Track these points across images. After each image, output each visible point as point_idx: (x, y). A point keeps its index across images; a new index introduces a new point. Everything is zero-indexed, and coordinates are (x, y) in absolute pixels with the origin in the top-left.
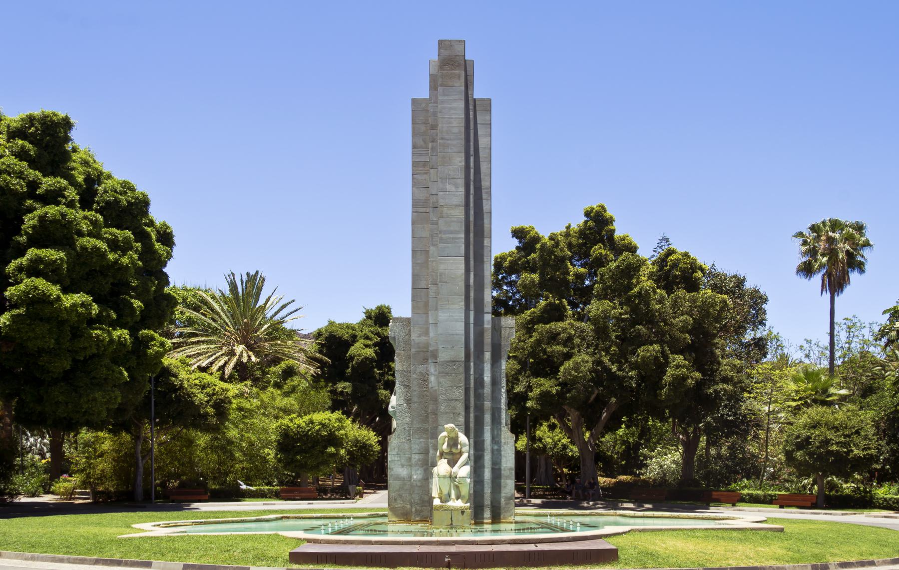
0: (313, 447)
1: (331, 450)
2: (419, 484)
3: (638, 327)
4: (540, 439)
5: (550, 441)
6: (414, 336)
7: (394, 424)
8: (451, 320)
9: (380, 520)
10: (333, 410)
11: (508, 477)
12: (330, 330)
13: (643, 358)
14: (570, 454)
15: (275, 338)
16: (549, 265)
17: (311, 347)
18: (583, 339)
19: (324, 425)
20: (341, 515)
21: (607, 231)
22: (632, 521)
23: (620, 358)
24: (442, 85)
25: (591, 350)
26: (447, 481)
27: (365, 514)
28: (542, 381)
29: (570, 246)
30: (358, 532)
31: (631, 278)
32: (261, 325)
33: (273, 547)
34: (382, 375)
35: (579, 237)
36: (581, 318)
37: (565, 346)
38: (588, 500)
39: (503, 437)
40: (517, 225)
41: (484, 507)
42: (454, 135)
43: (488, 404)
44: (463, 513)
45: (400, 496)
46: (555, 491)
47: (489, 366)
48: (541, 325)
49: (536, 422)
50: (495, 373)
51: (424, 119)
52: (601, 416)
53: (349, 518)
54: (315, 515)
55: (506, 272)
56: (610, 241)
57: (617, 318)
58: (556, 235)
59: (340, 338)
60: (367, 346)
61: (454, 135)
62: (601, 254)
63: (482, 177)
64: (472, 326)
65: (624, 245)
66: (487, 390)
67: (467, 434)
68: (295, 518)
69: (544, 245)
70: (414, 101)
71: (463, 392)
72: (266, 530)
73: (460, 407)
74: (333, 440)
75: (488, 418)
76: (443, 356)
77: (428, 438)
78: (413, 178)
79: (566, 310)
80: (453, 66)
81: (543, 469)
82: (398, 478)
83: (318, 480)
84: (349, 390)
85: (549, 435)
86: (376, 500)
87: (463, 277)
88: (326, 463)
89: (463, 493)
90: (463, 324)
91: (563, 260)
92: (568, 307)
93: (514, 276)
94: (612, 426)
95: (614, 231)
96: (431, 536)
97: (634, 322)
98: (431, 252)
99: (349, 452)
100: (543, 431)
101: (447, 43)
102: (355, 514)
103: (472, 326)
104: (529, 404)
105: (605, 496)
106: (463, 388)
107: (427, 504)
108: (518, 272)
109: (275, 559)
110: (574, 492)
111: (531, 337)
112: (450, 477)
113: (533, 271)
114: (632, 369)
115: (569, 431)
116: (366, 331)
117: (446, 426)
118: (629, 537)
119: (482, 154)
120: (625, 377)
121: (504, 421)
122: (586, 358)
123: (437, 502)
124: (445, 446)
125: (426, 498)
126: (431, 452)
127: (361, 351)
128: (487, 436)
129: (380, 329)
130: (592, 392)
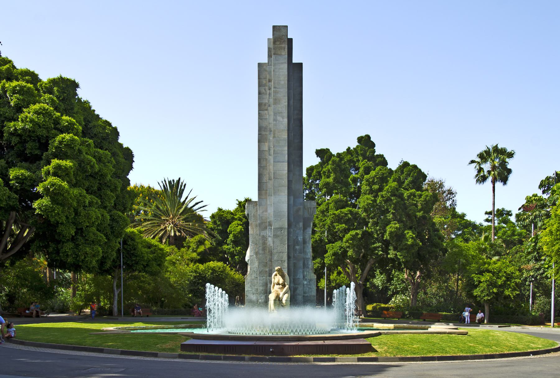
8: (280, 201)
49: (330, 271)
76: (275, 225)
78: (259, 113)
80: (281, 41)
101: (278, 28)
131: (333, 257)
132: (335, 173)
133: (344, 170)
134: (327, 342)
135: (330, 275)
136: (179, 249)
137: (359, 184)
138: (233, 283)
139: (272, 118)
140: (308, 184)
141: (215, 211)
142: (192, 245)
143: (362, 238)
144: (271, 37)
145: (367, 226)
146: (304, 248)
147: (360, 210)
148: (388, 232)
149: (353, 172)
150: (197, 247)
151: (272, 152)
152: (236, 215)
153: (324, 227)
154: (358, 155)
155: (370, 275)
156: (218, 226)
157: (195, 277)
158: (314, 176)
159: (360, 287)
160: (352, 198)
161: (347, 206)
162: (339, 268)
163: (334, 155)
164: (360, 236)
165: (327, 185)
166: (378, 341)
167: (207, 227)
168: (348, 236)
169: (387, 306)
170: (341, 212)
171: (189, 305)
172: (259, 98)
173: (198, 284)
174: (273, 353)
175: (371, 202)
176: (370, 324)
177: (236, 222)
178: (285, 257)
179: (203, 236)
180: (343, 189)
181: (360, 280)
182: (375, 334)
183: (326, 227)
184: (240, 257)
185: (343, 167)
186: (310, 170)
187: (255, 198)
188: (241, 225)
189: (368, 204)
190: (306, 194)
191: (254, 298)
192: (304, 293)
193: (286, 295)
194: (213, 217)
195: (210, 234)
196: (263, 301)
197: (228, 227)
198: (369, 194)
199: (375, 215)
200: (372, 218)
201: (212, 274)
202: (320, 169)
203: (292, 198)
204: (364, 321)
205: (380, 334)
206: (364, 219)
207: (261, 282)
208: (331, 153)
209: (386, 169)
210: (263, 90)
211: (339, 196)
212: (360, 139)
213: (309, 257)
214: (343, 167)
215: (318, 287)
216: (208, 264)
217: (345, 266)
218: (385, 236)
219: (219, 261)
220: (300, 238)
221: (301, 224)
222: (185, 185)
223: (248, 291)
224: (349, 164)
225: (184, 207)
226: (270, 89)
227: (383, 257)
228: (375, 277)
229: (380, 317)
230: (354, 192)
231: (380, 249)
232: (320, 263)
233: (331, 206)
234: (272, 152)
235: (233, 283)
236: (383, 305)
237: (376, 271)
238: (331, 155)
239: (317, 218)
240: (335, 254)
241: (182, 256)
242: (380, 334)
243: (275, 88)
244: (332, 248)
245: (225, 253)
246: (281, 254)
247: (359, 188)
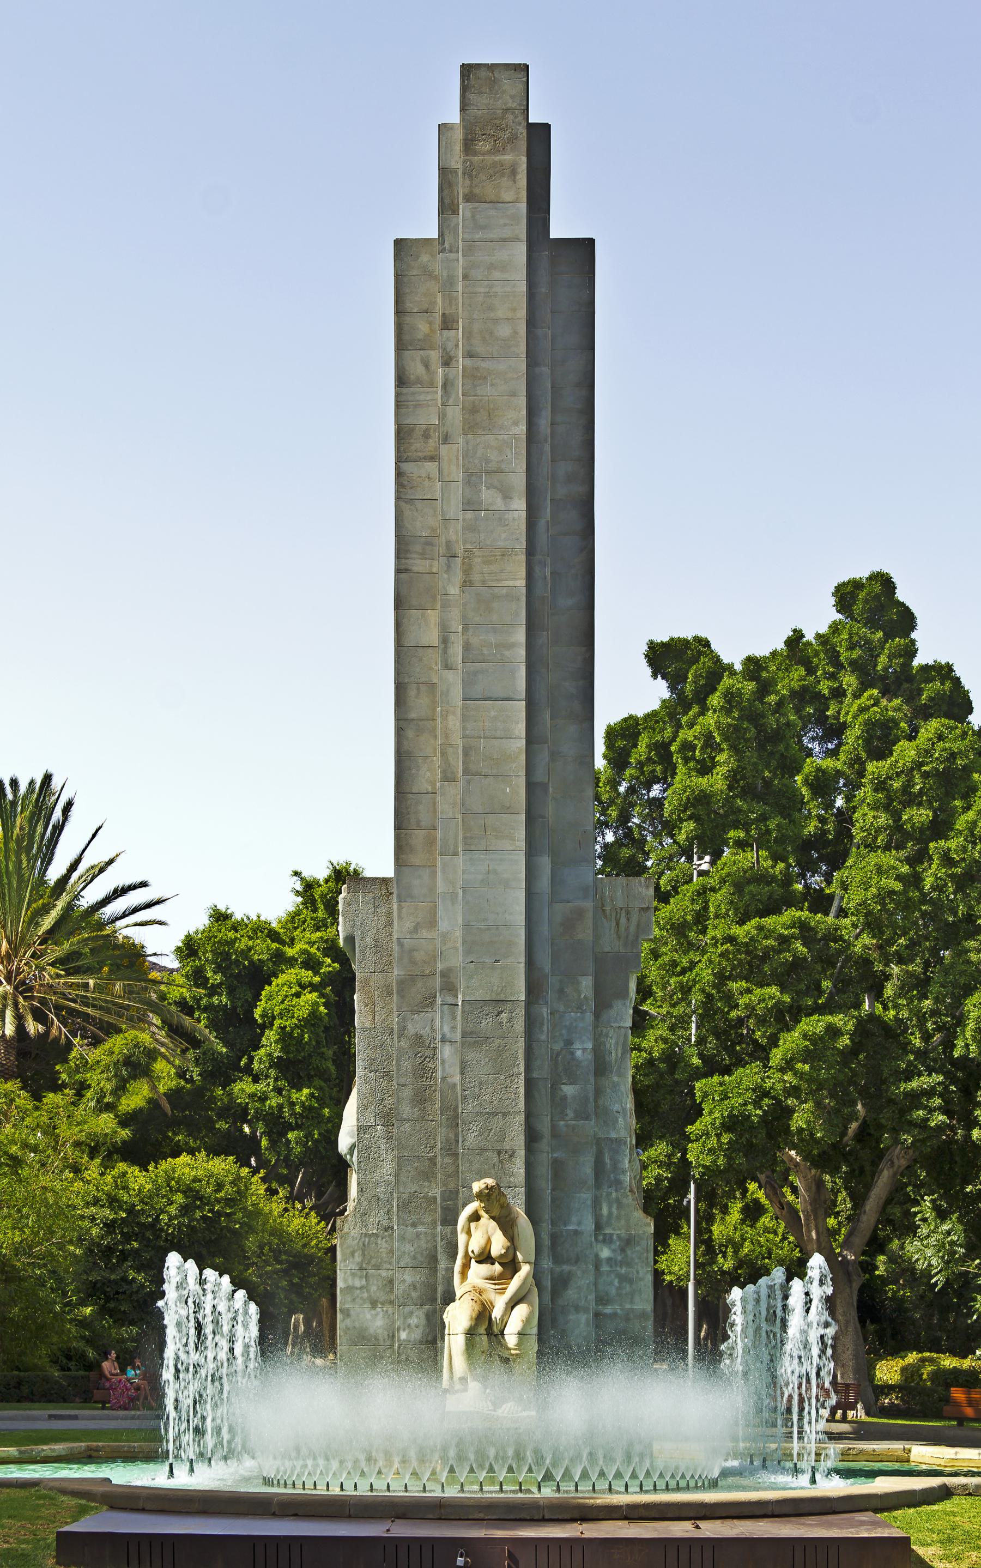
8: (495, 879)
49: (712, 1201)
78: (399, 474)
80: (499, 137)
131: (725, 1138)
132: (734, 748)
133: (777, 736)
134: (711, 1529)
135: (710, 1219)
136: (37, 1097)
137: (840, 802)
138: (277, 1253)
139: (457, 493)
140: (612, 802)
141: (199, 921)
142: (93, 1077)
143: (853, 1052)
144: (454, 116)
145: (877, 992)
146: (598, 1092)
147: (847, 922)
148: (971, 1025)
149: (816, 747)
150: (121, 1089)
151: (457, 650)
152: (292, 942)
153: (685, 999)
154: (839, 666)
155: (890, 1222)
156: (213, 990)
157: (109, 1226)
158: (641, 765)
159: (848, 1275)
160: (807, 866)
161: (790, 901)
162: (752, 1186)
163: (729, 668)
164: (846, 1041)
165: (699, 803)
166: (940, 1525)
167: (163, 997)
168: (791, 1041)
169: (966, 1363)
170: (760, 928)
171: (83, 1356)
172: (399, 405)
173: (124, 1256)
175: (898, 886)
176: (896, 1446)
177: (289, 975)
178: (517, 1139)
179: (145, 1038)
180: (772, 824)
181: (846, 1244)
182: (926, 1492)
183: (696, 998)
184: (309, 1135)
185: (772, 721)
186: (626, 732)
187: (378, 862)
188: (313, 987)
189: (884, 896)
190: (606, 846)
191: (375, 1322)
192: (602, 1300)
193: (521, 1311)
194: (189, 949)
195: (175, 1030)
196: (417, 1335)
197: (257, 997)
198: (887, 848)
199: (913, 944)
200: (901, 961)
201: (185, 1210)
202: (668, 732)
203: (545, 862)
204: (862, 1432)
205: (945, 1493)
206: (866, 962)
207: (408, 1248)
208: (717, 660)
209: (964, 734)
210: (416, 369)
211: (748, 858)
212: (846, 595)
213: (623, 1134)
214: (772, 721)
215: (658, 1275)
216: (164, 1165)
217: (776, 1182)
218: (960, 1043)
219: (214, 1151)
220: (582, 1050)
221: (586, 985)
223: (349, 1289)
224: (798, 710)
225: (61, 904)
226: (447, 362)
227: (951, 1141)
228: (911, 1230)
229: (939, 1416)
230: (818, 840)
231: (937, 1101)
232: (667, 1165)
233: (718, 900)
234: (457, 650)
235: (277, 1253)
236: (949, 1362)
237: (916, 1203)
238: (719, 669)
239: (656, 955)
240: (733, 1123)
241: (50, 1130)
242: (945, 1493)
243: (470, 355)
244: (723, 1097)
245: (241, 1114)
246: (497, 1122)
247: (844, 818)
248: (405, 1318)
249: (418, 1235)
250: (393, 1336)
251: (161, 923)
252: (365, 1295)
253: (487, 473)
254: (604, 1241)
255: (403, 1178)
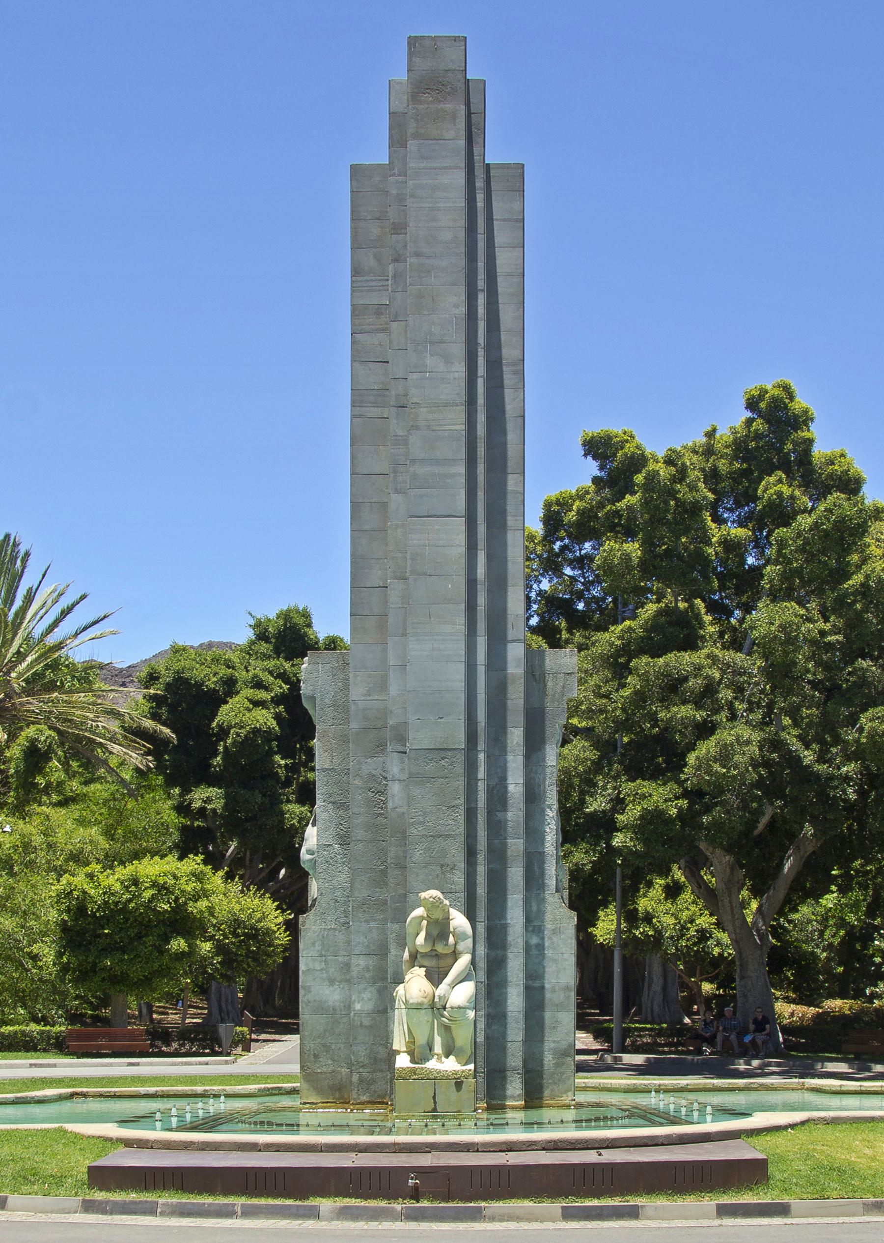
0: (139, 937)
1: (178, 944)
2: (366, 1022)
3: (864, 663)
4: (648, 918)
5: (670, 921)
6: (357, 692)
7: (314, 888)
8: (436, 660)
9: (286, 1102)
10: (184, 851)
11: (560, 1007)
12: (176, 667)
13: (873, 734)
14: (716, 951)
15: (51, 687)
16: (662, 521)
17: (133, 703)
18: (739, 690)
19: (162, 889)
20: (199, 1089)
21: (795, 443)
22: (835, 1101)
23: (824, 734)
24: (416, 136)
25: (757, 716)
26: (425, 1017)
27: (253, 1087)
28: (645, 786)
29: (712, 476)
30: (224, 1127)
31: (848, 551)
32: (20, 656)
33: (54, 1155)
34: (293, 769)
35: (735, 457)
36: (737, 641)
37: (698, 706)
38: (748, 1052)
39: (548, 917)
40: (596, 429)
41: (504, 1073)
42: (443, 250)
43: (516, 845)
44: (459, 1085)
45: (326, 1047)
46: (680, 1035)
47: (520, 759)
48: (645, 659)
49: (637, 880)
50: (535, 774)
51: (377, 210)
52: (781, 865)
53: (216, 1096)
54: (142, 1090)
55: (569, 536)
56: (801, 467)
57: (813, 642)
58: (679, 455)
59: (199, 685)
60: (258, 703)
61: (443, 250)
62: (779, 494)
63: (503, 337)
64: (481, 671)
65: (831, 476)
66: (515, 814)
67: (471, 916)
68: (101, 1095)
69: (652, 477)
70: (356, 171)
71: (461, 819)
72: (38, 1121)
73: (456, 853)
74: (181, 922)
75: (516, 875)
77: (384, 921)
78: (354, 342)
79: (702, 625)
80: (442, 93)
81: (657, 987)
82: (320, 1008)
83: (151, 1012)
84: (218, 805)
85: (671, 910)
86: (275, 1057)
87: (463, 561)
88: (165, 972)
89: (459, 1043)
90: (462, 667)
91: (695, 510)
92: (708, 618)
93: (588, 545)
94: (809, 886)
95: (811, 442)
96: (390, 1132)
97: (853, 650)
98: (392, 506)
99: (220, 949)
100: (650, 900)
102: (229, 1089)
103: (481, 671)
104: (618, 840)
105: (790, 1046)
106: (462, 811)
107: (384, 1067)
108: (595, 535)
109: (58, 1181)
110: (719, 1038)
111: (623, 686)
112: (432, 1006)
113: (629, 533)
114: (848, 758)
115: (710, 898)
116: (258, 668)
117: (423, 895)
118: (801, 1135)
119: (503, 286)
120: (831, 778)
121: (551, 882)
122: (746, 733)
123: (403, 1061)
124: (421, 939)
125: (382, 1053)
126: (393, 951)
127: (244, 715)
128: (515, 916)
129: (287, 665)
130: (759, 812)
174: (416, 1195)
222: (27, 554)
248: (359, 993)
249: (370, 929)
250: (349, 1007)
251: (83, 597)
252: (325, 975)
253: (431, 343)
254: (533, 931)
255: (357, 885)
